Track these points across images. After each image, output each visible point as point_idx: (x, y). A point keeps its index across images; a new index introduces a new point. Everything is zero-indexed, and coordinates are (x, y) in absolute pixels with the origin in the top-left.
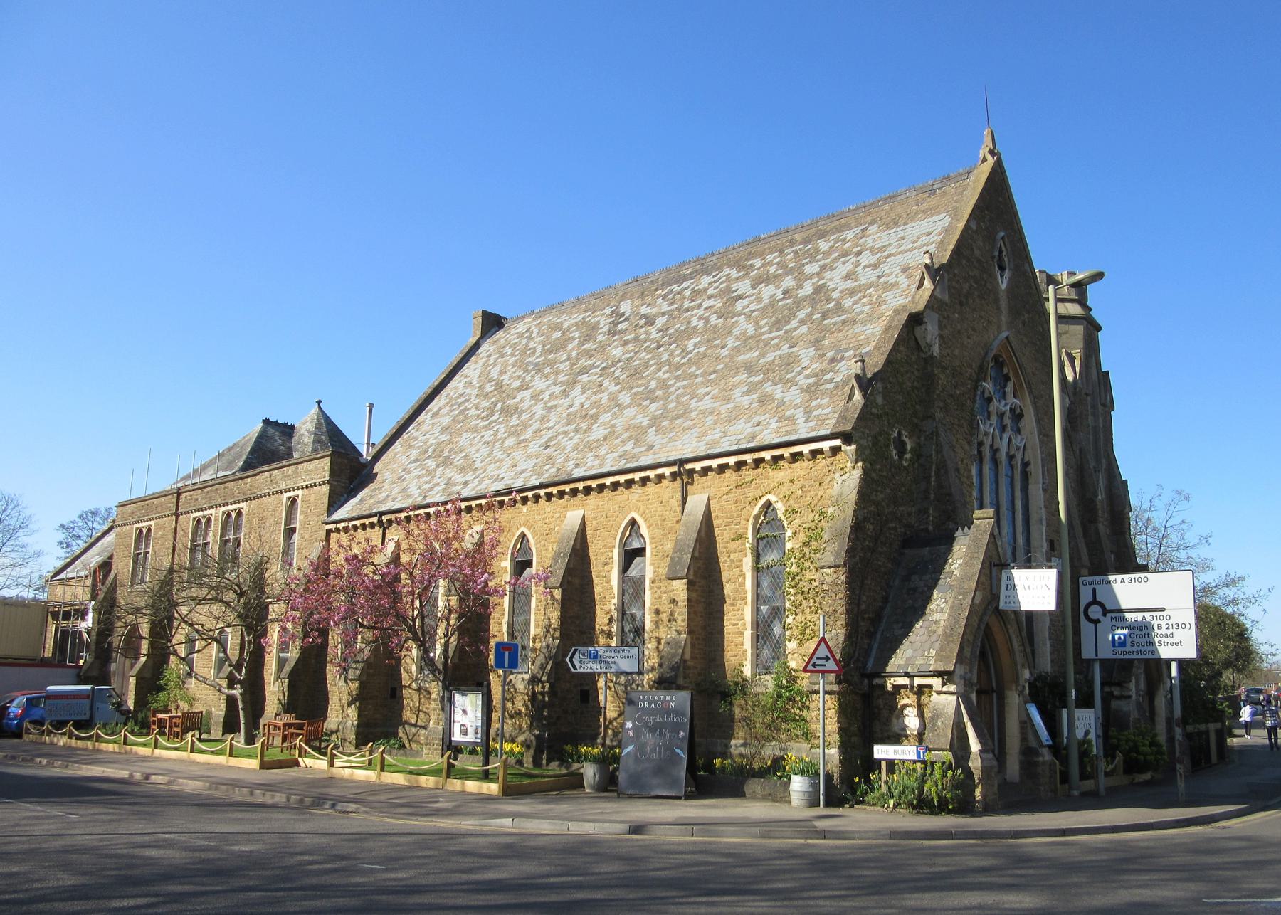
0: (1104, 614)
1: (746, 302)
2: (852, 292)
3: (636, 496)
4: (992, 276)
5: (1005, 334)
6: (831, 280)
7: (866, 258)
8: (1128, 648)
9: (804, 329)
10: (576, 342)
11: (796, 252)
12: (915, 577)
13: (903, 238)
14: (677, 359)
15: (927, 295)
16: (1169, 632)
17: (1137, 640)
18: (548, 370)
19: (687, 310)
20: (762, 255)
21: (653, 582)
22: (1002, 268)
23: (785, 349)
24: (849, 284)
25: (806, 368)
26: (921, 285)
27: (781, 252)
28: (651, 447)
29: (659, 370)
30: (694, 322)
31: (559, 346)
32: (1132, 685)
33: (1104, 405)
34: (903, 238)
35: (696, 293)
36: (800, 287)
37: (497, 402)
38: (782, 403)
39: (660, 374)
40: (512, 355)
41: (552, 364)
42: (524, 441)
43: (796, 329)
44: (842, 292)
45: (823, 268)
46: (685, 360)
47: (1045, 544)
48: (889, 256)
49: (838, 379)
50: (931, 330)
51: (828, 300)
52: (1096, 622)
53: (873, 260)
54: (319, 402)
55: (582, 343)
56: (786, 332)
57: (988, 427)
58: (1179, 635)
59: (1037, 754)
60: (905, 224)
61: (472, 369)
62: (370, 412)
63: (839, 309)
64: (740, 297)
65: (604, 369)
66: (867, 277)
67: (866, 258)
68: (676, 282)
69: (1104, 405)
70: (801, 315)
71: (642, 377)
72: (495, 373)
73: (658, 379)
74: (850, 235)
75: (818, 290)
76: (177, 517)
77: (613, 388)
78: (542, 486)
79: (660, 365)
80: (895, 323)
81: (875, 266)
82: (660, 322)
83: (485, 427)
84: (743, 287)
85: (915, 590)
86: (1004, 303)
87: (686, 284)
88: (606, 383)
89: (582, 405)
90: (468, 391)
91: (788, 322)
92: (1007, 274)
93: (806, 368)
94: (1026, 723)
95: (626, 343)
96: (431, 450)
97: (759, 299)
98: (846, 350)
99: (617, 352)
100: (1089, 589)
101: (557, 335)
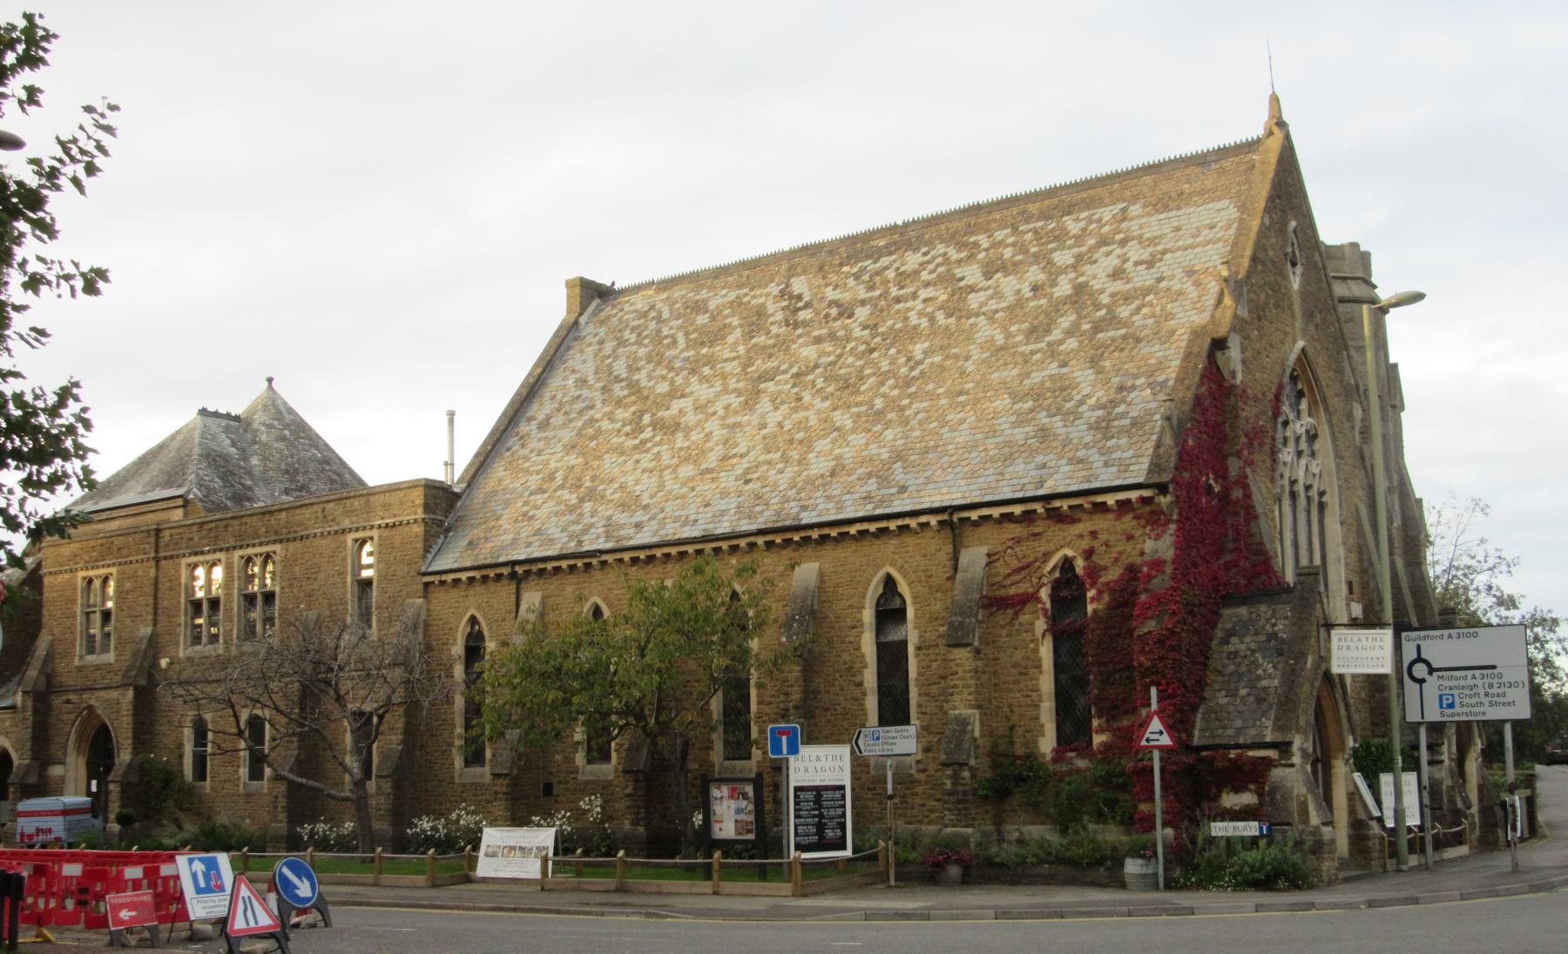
0: (1430, 673)
1: (982, 296)
2: (1127, 298)
3: (891, 548)
4: (1285, 277)
5: (1301, 344)
6: (1094, 277)
7: (1135, 252)
8: (1457, 709)
9: (1072, 344)
10: (738, 333)
11: (1035, 231)
12: (1234, 640)
13: (1178, 229)
14: (904, 370)
15: (1229, 314)
16: (1500, 691)
17: (1467, 701)
18: (706, 371)
19: (898, 300)
20: (988, 230)
21: (919, 648)
22: (1294, 264)
23: (1053, 368)
24: (1119, 286)
25: (1088, 396)
26: (1219, 301)
27: (1015, 229)
28: (903, 489)
29: (882, 383)
30: (914, 319)
31: (717, 335)
32: (1445, 748)
33: (1394, 407)
34: (1178, 229)
35: (903, 278)
36: (1054, 283)
37: (642, 412)
38: (1067, 442)
39: (884, 389)
40: (639, 343)
41: (711, 361)
42: (708, 471)
43: (1061, 342)
44: (1112, 295)
45: (1079, 258)
46: (916, 373)
47: (1344, 588)
48: (1164, 252)
49: (1133, 414)
50: (1234, 355)
51: (1098, 307)
52: (1421, 681)
53: (1145, 255)
54: (270, 380)
55: (749, 335)
56: (1050, 345)
57: (1287, 455)
58: (1512, 694)
59: (1368, 827)
60: (1179, 208)
61: (582, 360)
62: (451, 422)
63: (1112, 320)
64: (972, 289)
65: (797, 375)
66: (1142, 278)
67: (1135, 252)
68: (868, 257)
69: (1394, 407)
70: (1065, 322)
71: (857, 392)
72: (620, 369)
73: (884, 396)
74: (1106, 214)
75: (1080, 289)
76: (157, 560)
77: (819, 404)
78: (761, 532)
79: (883, 377)
80: (1195, 350)
81: (1150, 264)
82: (862, 313)
83: (635, 447)
84: (971, 274)
85: (1236, 653)
86: (1297, 309)
87: (885, 261)
88: (807, 397)
89: (780, 425)
90: (585, 393)
91: (1048, 332)
92: (1299, 269)
93: (1088, 396)
94: (1354, 796)
95: (818, 340)
96: (559, 476)
97: (998, 294)
98: (1136, 377)
99: (809, 353)
100: (1413, 645)
101: (702, 319)
